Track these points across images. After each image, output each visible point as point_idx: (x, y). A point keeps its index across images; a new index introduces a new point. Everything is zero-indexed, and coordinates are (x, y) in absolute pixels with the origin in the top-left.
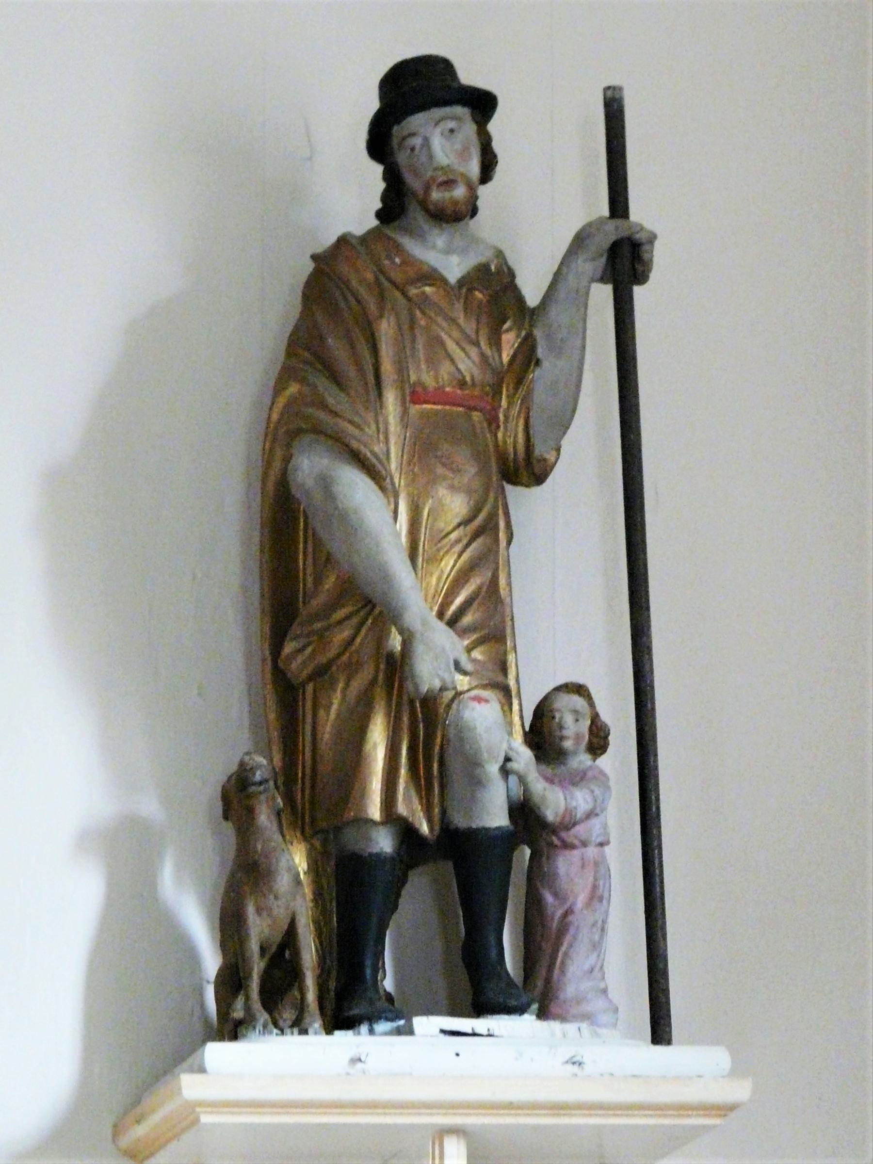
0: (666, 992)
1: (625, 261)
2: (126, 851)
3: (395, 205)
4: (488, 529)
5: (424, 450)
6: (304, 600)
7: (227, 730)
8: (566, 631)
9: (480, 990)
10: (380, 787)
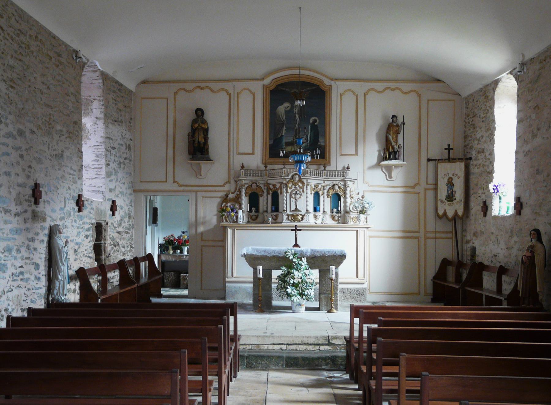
0: (418, 147)
1: (404, 123)
2: (379, 151)
3: (393, 121)
4: (397, 137)
5: (393, 134)
6: (387, 139)
7: (385, 147)
8: (400, 142)
9: (395, 159)
10: (391, 150)
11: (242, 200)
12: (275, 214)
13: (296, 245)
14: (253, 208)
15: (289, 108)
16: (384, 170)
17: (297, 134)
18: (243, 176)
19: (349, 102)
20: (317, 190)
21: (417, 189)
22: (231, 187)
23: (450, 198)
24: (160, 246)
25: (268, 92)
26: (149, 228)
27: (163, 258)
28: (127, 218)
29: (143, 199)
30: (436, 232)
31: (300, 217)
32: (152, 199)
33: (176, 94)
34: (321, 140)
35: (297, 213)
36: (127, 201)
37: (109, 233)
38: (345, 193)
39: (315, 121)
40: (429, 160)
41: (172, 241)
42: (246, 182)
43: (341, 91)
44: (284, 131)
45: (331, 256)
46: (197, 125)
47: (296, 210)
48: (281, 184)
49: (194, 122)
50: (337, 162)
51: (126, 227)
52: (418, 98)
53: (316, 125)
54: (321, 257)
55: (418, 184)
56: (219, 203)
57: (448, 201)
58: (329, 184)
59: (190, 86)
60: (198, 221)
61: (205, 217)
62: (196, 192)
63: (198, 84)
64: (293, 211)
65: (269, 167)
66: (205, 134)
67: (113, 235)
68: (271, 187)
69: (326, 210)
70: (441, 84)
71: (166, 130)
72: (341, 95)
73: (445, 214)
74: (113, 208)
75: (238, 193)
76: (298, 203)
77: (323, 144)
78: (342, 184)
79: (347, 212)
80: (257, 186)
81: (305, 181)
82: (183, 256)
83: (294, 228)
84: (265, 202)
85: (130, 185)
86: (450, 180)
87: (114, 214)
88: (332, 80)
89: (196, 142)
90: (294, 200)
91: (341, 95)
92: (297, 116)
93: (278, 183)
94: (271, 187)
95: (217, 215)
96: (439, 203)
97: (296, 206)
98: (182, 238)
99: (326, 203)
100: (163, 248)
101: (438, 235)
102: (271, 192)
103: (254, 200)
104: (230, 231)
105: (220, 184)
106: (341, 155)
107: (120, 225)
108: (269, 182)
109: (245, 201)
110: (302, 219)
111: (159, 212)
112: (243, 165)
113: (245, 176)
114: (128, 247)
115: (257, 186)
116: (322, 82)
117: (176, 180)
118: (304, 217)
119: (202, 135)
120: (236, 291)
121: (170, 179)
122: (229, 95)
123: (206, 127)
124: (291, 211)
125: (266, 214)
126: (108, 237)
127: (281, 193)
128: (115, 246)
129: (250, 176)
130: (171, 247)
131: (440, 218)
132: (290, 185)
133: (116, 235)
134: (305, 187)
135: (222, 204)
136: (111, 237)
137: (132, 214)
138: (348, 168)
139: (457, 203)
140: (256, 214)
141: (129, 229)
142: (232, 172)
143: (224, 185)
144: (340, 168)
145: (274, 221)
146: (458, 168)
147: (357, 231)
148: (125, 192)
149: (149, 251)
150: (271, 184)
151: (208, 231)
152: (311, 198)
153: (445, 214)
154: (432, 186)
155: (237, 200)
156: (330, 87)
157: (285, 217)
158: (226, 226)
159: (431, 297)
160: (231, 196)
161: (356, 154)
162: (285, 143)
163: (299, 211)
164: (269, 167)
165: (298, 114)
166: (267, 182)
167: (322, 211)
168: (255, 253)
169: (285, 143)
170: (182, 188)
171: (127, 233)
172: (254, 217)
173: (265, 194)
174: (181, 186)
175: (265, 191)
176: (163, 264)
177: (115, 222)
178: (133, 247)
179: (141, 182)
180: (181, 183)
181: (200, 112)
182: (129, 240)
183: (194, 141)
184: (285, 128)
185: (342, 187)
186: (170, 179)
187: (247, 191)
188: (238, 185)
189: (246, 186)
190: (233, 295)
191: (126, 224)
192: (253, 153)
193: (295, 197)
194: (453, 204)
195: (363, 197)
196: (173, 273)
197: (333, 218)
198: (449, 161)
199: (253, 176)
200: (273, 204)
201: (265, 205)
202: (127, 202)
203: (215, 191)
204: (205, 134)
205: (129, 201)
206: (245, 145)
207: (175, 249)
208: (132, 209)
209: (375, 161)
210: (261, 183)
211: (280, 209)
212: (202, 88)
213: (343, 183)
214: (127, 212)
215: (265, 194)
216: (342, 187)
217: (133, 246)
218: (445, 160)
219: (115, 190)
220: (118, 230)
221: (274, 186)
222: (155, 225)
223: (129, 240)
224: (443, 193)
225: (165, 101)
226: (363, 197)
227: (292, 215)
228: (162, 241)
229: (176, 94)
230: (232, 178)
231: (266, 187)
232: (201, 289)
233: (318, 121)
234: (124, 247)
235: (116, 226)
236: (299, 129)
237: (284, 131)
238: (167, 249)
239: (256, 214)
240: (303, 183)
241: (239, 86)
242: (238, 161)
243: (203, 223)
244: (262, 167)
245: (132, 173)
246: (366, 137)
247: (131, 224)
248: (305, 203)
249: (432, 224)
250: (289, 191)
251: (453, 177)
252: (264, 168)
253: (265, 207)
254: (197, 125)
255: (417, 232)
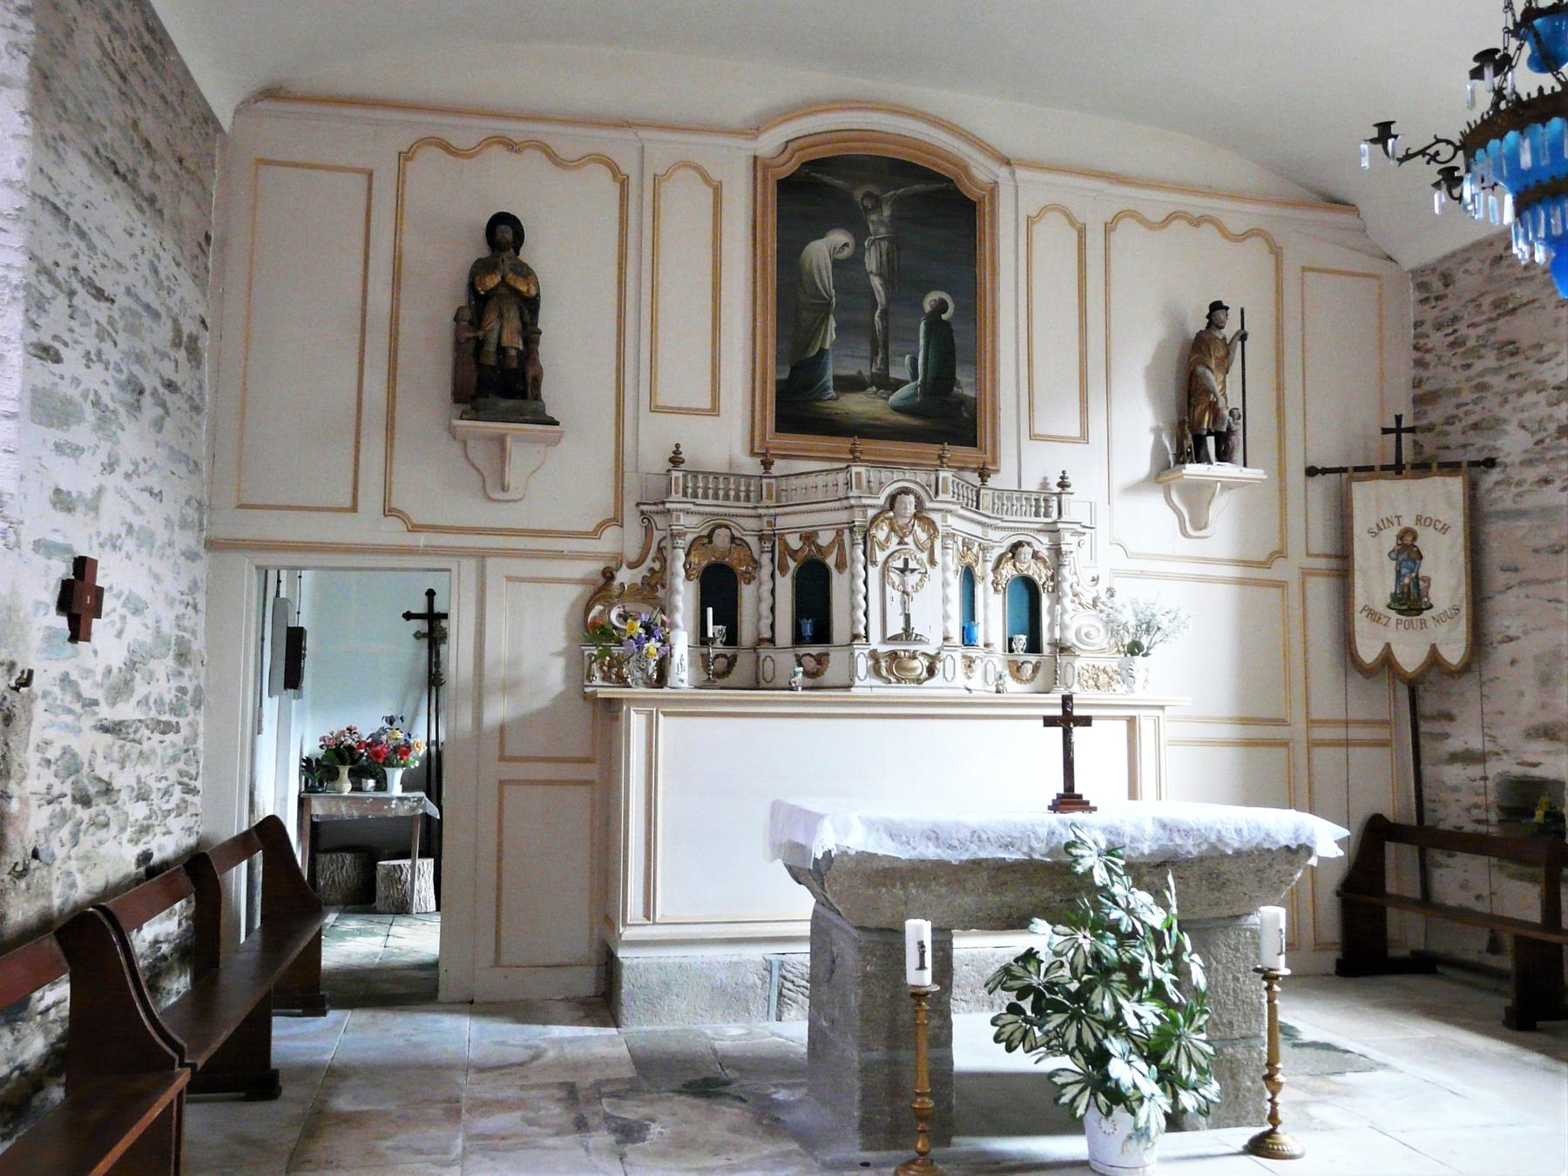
2: (1157, 432)
8: (1234, 401)
9: (1224, 455)
11: (672, 591)
12: (815, 650)
13: (1069, 800)
15: (847, 252)
16: (1175, 497)
17: (880, 346)
18: (679, 497)
19: (1054, 248)
21: (1278, 571)
22: (629, 540)
23: (1410, 601)
24: (308, 766)
25: (772, 187)
26: (271, 705)
27: (318, 808)
28: (170, 661)
29: (252, 582)
30: (1347, 723)
31: (920, 665)
32: (283, 595)
33: (405, 157)
34: (962, 376)
35: (912, 648)
36: (168, 576)
37: (35, 736)
39: (941, 306)
40: (1311, 472)
41: (350, 748)
42: (690, 523)
43: (1029, 206)
44: (832, 335)
45: (1250, 854)
46: (492, 281)
47: (907, 634)
48: (839, 533)
49: (480, 268)
50: (1023, 461)
51: (159, 702)
52: (1272, 256)
53: (947, 324)
54: (1201, 859)
55: (1280, 554)
56: (573, 606)
57: (1401, 612)
58: (1001, 541)
59: (465, 134)
60: (487, 681)
61: (515, 662)
62: (482, 555)
63: (501, 126)
64: (895, 638)
65: (779, 467)
66: (527, 318)
67: (76, 744)
70: (1345, 218)
71: (359, 300)
72: (1030, 221)
73: (1387, 660)
74: (78, 599)
75: (657, 566)
77: (969, 392)
78: (1043, 544)
80: (733, 538)
81: (936, 517)
82: (389, 800)
83: (1059, 712)
84: (768, 601)
85: (192, 514)
86: (1408, 539)
87: (78, 632)
88: (1007, 162)
89: (492, 348)
91: (1030, 221)
92: (876, 282)
94: (794, 542)
95: (564, 653)
96: (1361, 623)
97: (907, 617)
98: (384, 738)
99: (994, 613)
100: (318, 773)
101: (1356, 733)
102: (792, 564)
103: (719, 589)
105: (584, 529)
106: (1033, 437)
107: (121, 690)
108: (781, 522)
109: (685, 595)
110: (931, 671)
111: (310, 643)
113: (685, 494)
114: (167, 793)
115: (733, 538)
116: (965, 168)
117: (395, 505)
118: (939, 665)
119: (513, 323)
120: (666, 985)
121: (371, 499)
122: (624, 184)
123: (533, 292)
124: (886, 640)
126: (32, 757)
128: (85, 801)
129: (706, 496)
130: (344, 771)
131: (1368, 672)
133: (89, 744)
134: (938, 544)
135: (588, 610)
136: (53, 753)
137: (195, 646)
138: (1063, 484)
139: (1437, 620)
141: (174, 711)
142: (630, 481)
143: (596, 533)
144: (1031, 484)
145: (810, 682)
146: (1441, 497)
147: (1131, 721)
148: (162, 536)
149: (266, 808)
150: (792, 530)
151: (527, 722)
152: (955, 583)
153: (1387, 660)
154: (1322, 563)
155: (654, 588)
156: (993, 189)
157: (863, 664)
159: (1337, 954)
160: (624, 577)
161: (1084, 437)
162: (836, 378)
163: (919, 640)
165: (880, 275)
167: (980, 642)
168: (886, 848)
169: (836, 378)
170: (422, 540)
171: (166, 728)
172: (721, 664)
174: (416, 528)
176: (315, 832)
177: (88, 673)
178: (194, 791)
179: (241, 506)
180: (417, 519)
181: (504, 233)
182: (175, 759)
183: (480, 344)
184: (832, 323)
185: (1044, 553)
186: (371, 499)
187: (694, 559)
188: (657, 535)
189: (690, 537)
190: (652, 1004)
191: (164, 688)
192: (714, 410)
193: (903, 583)
194: (1423, 623)
196: (348, 858)
198: (1399, 473)
199: (716, 497)
200: (800, 612)
201: (776, 616)
202: (174, 585)
203: (559, 555)
204: (527, 318)
205: (184, 584)
206: (683, 378)
207: (357, 775)
208: (197, 621)
209: (1142, 464)
210: (748, 527)
212: (511, 146)
213: (1045, 539)
214: (168, 628)
217: (198, 784)
218: (1384, 468)
219: (94, 507)
220: (106, 713)
221: (809, 537)
222: (291, 691)
223: (175, 759)
224: (1375, 581)
225: (362, 180)
227: (894, 655)
228: (313, 749)
229: (405, 157)
230: (629, 505)
231: (768, 545)
232: (497, 963)
233: (951, 310)
234: (142, 796)
235: (99, 695)
236: (886, 329)
237: (832, 335)
238: (333, 775)
239: (729, 651)
241: (663, 149)
242: (652, 440)
243: (510, 686)
244: (752, 466)
245: (204, 466)
246: (1113, 374)
247: (190, 687)
248: (933, 608)
249: (1328, 694)
250: (880, 556)
251: (1417, 528)
252: (760, 470)
253: (766, 622)
254: (492, 281)
255: (1280, 722)
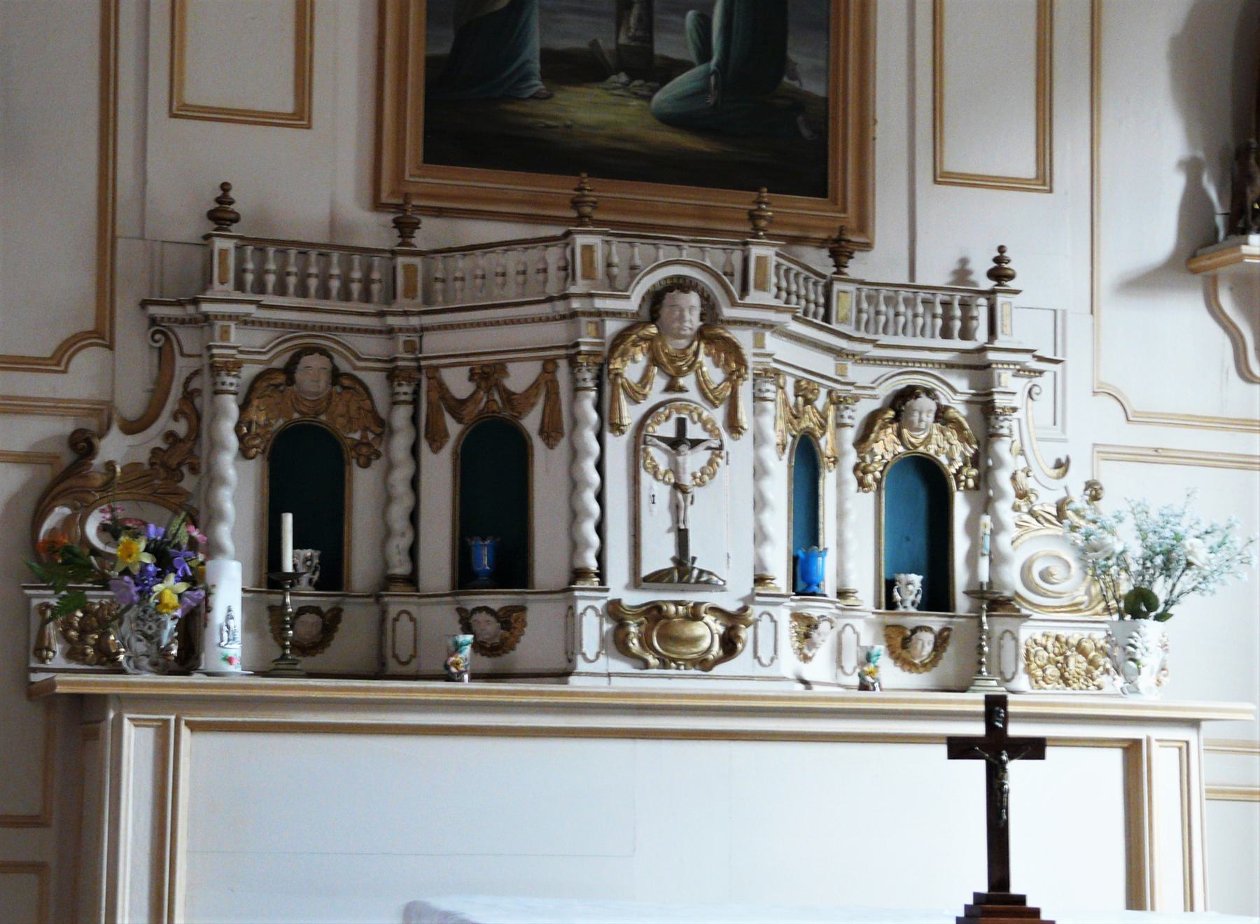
2: (1192, 168)
11: (213, 480)
12: (497, 600)
14: (476, 542)
16: (1226, 302)
18: (228, 290)
20: (809, 421)
22: (125, 374)
31: (707, 632)
34: (800, 55)
35: (691, 597)
38: (983, 461)
42: (248, 344)
47: (682, 570)
48: (549, 366)
50: (923, 231)
58: (873, 385)
64: (658, 578)
65: (431, 232)
68: (458, 383)
69: (851, 585)
75: (181, 428)
76: (694, 520)
77: (814, 87)
78: (956, 393)
79: (994, 601)
80: (336, 376)
81: (743, 337)
84: (406, 500)
90: (663, 492)
93: (522, 353)
94: (458, 383)
97: (682, 538)
102: (454, 428)
104: (135, 743)
106: (942, 177)
108: (434, 344)
109: (236, 488)
110: (730, 646)
112: (224, 198)
113: (240, 286)
115: (336, 376)
118: (746, 633)
124: (638, 581)
125: (412, 605)
127: (551, 432)
129: (281, 290)
132: (632, 370)
138: (1000, 273)
140: (325, 602)
142: (128, 256)
143: (59, 360)
144: (934, 273)
145: (486, 664)
147: (1132, 750)
150: (456, 360)
155: (175, 477)
157: (592, 629)
158: (100, 701)
160: (115, 449)
161: (1044, 179)
163: (706, 581)
164: (431, 232)
166: (411, 347)
173: (400, 445)
175: (401, 416)
185: (959, 410)
187: (258, 416)
188: (183, 367)
192: (300, 117)
193: (675, 469)
195: (1094, 492)
197: (900, 644)
199: (303, 291)
209: (1160, 235)
211: (547, 561)
213: (962, 384)
215: (400, 445)
216: (959, 410)
221: (487, 374)
226: (1094, 492)
227: (654, 612)
231: (405, 389)
239: (325, 602)
240: (731, 354)
242: (177, 171)
244: (374, 230)
248: (735, 520)
250: (630, 414)
253: (400, 543)
